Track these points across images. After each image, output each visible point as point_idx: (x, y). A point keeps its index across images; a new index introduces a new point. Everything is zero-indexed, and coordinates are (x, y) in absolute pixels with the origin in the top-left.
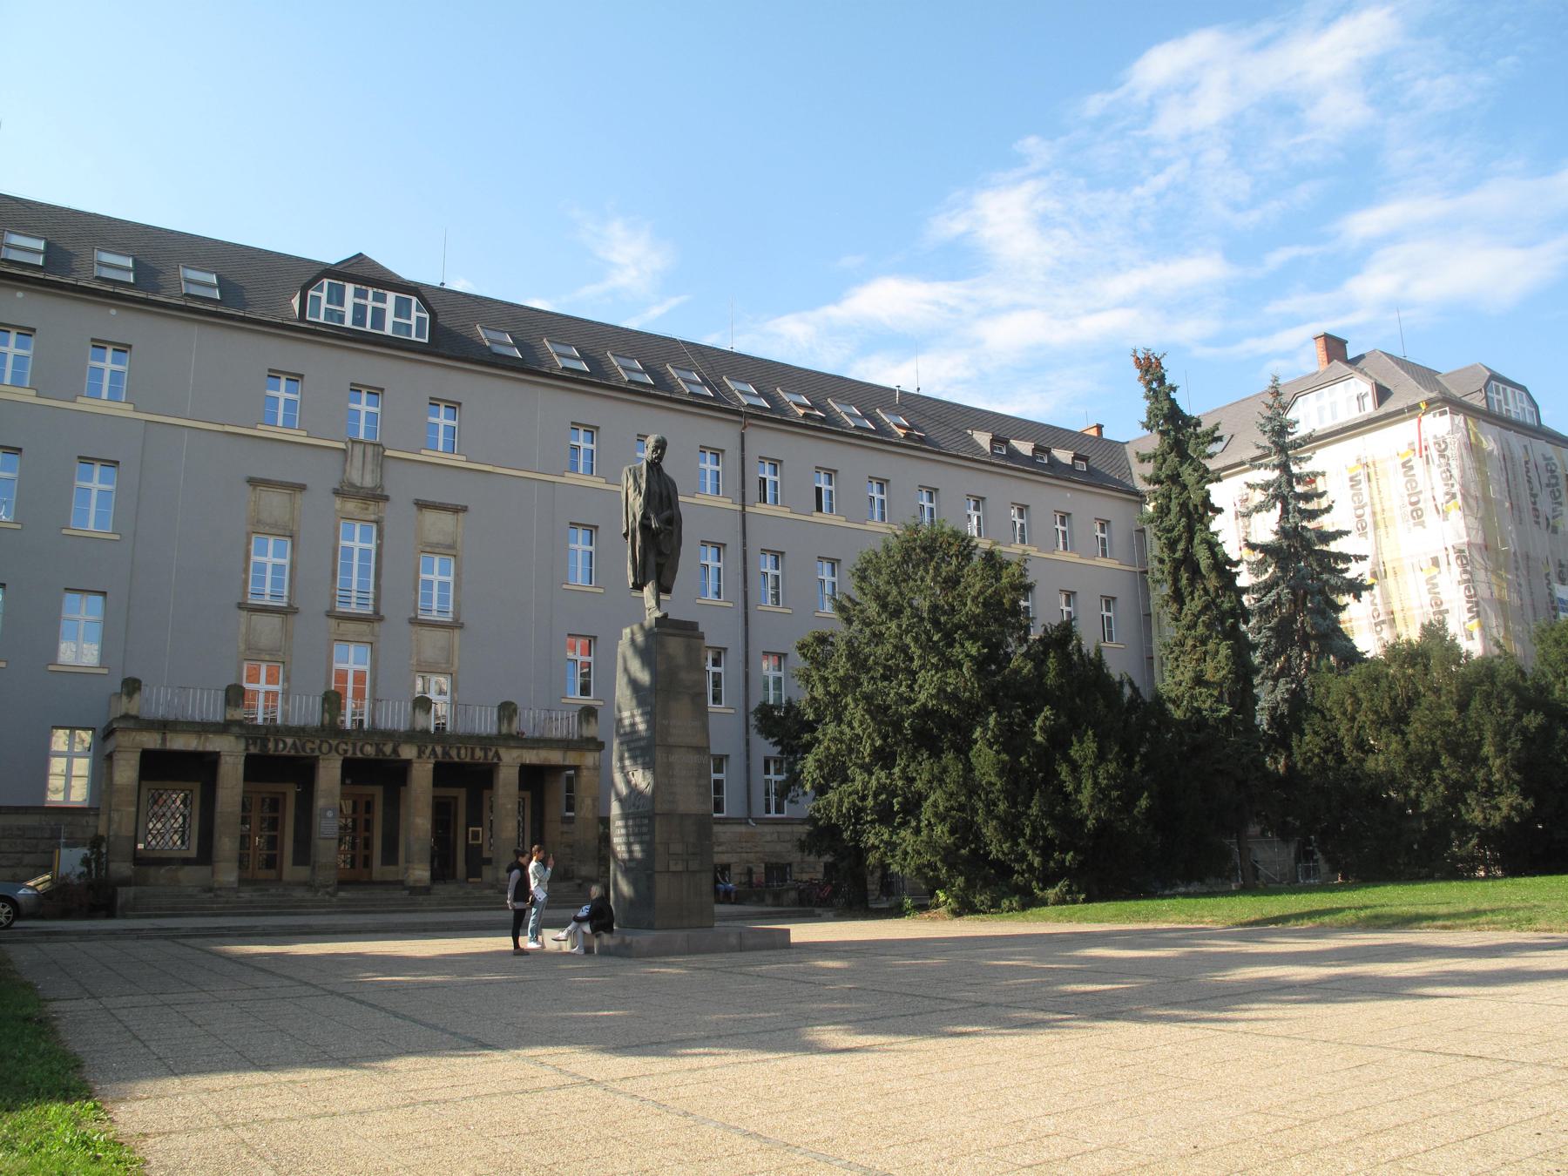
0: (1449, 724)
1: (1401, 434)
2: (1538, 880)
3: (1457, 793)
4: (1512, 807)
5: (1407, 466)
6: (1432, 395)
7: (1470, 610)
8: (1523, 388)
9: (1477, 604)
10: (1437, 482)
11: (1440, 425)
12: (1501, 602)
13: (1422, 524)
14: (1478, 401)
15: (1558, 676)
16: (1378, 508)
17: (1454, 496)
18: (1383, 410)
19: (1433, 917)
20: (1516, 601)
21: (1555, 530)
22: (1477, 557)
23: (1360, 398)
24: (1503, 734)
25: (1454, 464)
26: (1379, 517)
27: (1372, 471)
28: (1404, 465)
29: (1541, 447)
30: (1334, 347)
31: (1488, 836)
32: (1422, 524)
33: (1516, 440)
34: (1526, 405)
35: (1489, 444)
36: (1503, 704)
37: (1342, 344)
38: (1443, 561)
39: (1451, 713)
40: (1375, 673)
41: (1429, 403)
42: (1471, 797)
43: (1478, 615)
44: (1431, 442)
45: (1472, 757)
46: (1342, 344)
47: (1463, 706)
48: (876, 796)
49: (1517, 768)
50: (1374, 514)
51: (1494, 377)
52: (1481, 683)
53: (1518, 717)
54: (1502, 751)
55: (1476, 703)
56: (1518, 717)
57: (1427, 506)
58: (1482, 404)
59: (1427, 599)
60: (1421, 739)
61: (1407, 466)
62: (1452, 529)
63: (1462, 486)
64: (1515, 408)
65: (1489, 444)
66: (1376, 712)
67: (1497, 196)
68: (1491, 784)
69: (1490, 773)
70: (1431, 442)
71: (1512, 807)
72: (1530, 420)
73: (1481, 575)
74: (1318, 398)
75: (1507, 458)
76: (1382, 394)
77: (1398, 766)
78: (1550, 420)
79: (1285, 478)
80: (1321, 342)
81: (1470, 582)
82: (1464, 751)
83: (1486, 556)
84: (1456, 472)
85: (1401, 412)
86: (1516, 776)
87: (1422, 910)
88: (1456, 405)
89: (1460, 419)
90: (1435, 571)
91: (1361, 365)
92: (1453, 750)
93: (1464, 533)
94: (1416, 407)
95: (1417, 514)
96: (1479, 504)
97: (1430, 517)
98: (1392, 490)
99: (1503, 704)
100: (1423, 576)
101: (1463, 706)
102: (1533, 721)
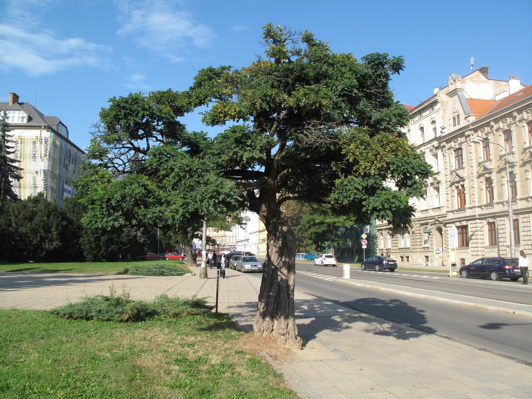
0: (44, 221)
1: (33, 133)
2: (68, 263)
3: (43, 239)
4: (56, 245)
5: (34, 143)
6: (46, 125)
7: (44, 188)
8: (66, 127)
9: (46, 187)
10: (41, 149)
11: (46, 134)
12: (52, 187)
13: (35, 161)
14: (55, 128)
15: (69, 211)
16: (23, 153)
17: (46, 155)
18: (29, 124)
19: (62, 270)
20: (55, 188)
21: (67, 170)
22: (49, 174)
23: (23, 118)
24: (58, 226)
25: (48, 146)
26: (22, 155)
27: (23, 141)
28: (33, 142)
29: (69, 146)
30: (16, 98)
31: (48, 252)
32: (35, 161)
33: (64, 143)
34: (66, 132)
35: (58, 143)
36: (58, 217)
37: (18, 97)
38: (39, 173)
39: (45, 219)
40: (24, 205)
41: (45, 127)
42: (47, 241)
43: (46, 190)
44: (43, 138)
45: (48, 230)
46: (18, 97)
47: (48, 217)
48: (107, 246)
49: (59, 235)
50: (21, 154)
51: (61, 123)
52: (53, 211)
53: (61, 221)
54: (57, 230)
55: (52, 217)
56: (61, 221)
57: (38, 155)
58: (56, 129)
59: (32, 182)
60: (36, 225)
61: (34, 143)
62: (43, 165)
63: (50, 153)
64: (63, 132)
65: (58, 143)
66: (24, 215)
67: (43, 40)
68: (52, 238)
69: (52, 235)
70: (43, 138)
71: (56, 245)
72: (66, 136)
73: (49, 179)
74: (13, 113)
75: (61, 147)
76: (30, 119)
77: (29, 231)
78: (70, 138)
79: (3, 140)
80: (12, 95)
81: (45, 180)
82: (47, 229)
83: (50, 175)
84: (48, 149)
85: (36, 126)
86: (58, 237)
87: (57, 269)
88: (49, 128)
89: (53, 134)
90: (36, 175)
91: (22, 106)
92: (44, 228)
93: (47, 166)
94: (41, 127)
95: (34, 157)
96: (52, 159)
97: (38, 160)
98: (28, 149)
99: (58, 217)
100: (32, 176)
101: (48, 217)
102: (65, 223)
